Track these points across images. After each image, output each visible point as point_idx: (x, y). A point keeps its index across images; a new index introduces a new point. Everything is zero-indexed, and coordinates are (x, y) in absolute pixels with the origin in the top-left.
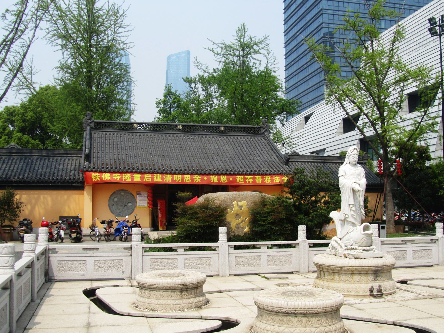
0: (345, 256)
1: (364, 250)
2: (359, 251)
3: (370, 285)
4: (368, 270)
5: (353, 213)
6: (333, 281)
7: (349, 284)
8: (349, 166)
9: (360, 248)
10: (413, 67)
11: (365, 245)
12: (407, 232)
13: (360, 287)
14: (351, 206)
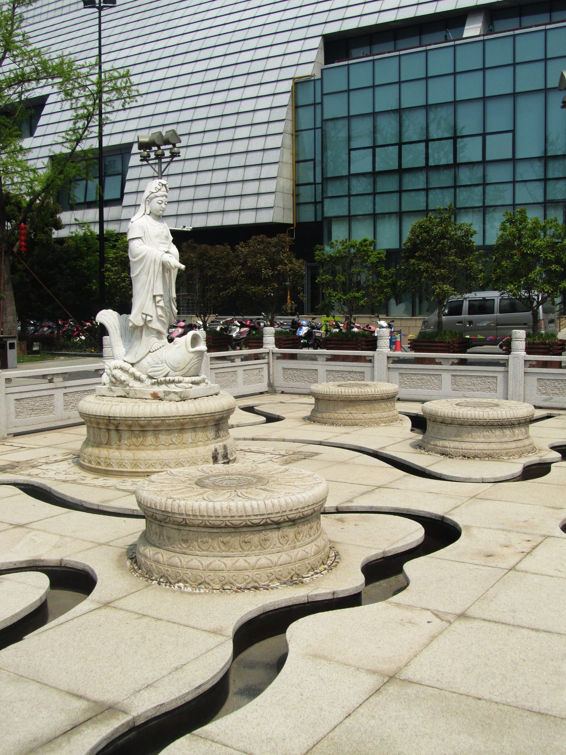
0: (155, 396)
1: (193, 383)
2: (186, 385)
3: (212, 447)
4: (209, 421)
5: (160, 312)
6: (142, 447)
7: (176, 451)
8: (150, 218)
9: (187, 379)
10: (53, 56)
11: (192, 374)
12: (37, 352)
13: (197, 453)
14: (158, 298)
